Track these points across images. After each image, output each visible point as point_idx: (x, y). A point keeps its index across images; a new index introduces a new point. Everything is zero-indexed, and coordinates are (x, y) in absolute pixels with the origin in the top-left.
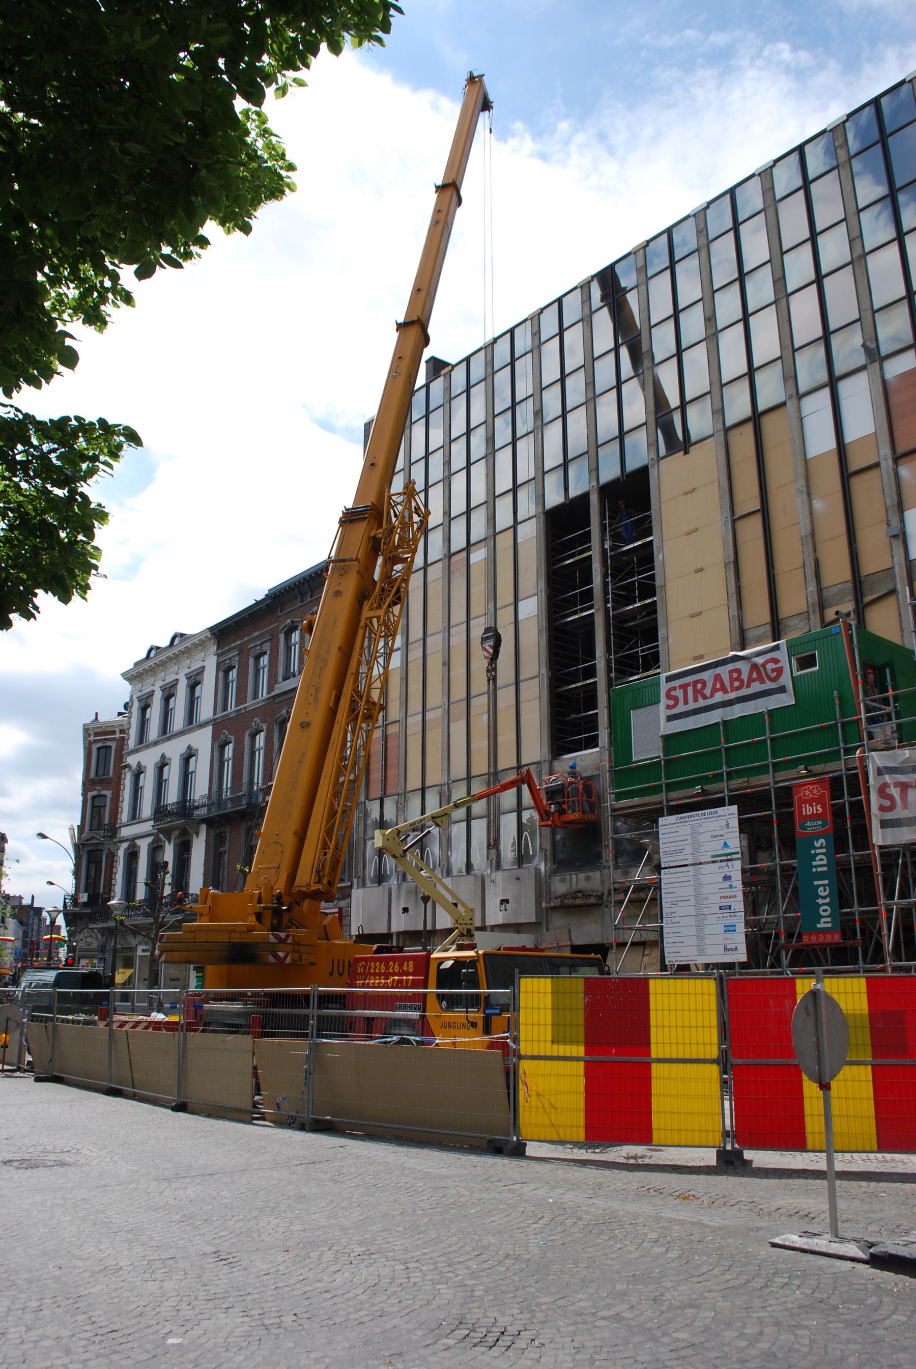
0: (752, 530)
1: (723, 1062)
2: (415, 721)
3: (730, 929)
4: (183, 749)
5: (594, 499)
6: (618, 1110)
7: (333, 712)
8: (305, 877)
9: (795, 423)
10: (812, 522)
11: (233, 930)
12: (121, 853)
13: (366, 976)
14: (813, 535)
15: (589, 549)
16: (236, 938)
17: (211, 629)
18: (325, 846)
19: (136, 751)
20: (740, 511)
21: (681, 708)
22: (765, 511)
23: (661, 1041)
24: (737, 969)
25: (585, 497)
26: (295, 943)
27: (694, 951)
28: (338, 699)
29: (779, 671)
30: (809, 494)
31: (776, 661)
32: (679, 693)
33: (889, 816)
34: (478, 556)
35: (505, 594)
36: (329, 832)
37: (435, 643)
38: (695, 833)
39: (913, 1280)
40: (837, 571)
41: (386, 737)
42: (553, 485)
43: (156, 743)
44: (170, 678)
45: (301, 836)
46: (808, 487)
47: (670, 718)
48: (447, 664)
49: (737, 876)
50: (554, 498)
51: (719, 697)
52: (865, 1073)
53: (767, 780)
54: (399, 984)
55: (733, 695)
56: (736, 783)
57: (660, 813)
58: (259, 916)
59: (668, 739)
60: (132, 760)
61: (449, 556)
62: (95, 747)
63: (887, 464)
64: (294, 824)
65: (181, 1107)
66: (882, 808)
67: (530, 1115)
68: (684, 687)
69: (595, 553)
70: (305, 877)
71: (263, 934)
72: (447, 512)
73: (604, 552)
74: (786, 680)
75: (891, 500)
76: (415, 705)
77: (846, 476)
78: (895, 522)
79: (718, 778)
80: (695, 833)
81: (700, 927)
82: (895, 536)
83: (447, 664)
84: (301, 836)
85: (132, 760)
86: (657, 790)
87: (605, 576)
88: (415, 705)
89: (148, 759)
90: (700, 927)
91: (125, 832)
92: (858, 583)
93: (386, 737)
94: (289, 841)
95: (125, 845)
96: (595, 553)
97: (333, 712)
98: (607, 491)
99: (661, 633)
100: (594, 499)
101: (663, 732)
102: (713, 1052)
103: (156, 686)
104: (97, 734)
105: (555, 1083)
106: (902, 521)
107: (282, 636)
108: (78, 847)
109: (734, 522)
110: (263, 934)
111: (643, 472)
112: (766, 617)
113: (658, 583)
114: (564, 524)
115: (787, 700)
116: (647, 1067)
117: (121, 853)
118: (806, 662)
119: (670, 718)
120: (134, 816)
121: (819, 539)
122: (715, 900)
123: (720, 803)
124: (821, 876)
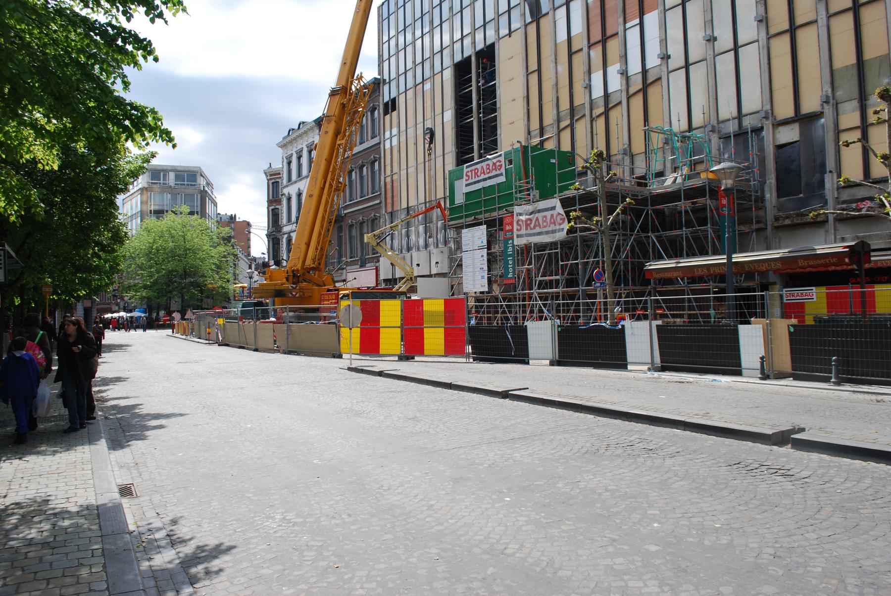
0: (534, 78)
1: (401, 327)
2: (404, 172)
3: (483, 277)
4: (297, 190)
5: (473, 59)
6: (370, 344)
7: (323, 189)
8: (309, 262)
9: (552, 24)
10: (557, 78)
11: (276, 285)
12: (284, 240)
13: (324, 300)
14: (557, 84)
15: (471, 86)
16: (277, 288)
17: (315, 121)
18: (317, 249)
19: (287, 186)
20: (530, 70)
21: (470, 181)
22: (539, 70)
23: (384, 320)
24: (682, 284)
25: (470, 57)
26: (300, 289)
27: (472, 287)
28: (325, 182)
29: (501, 166)
30: (556, 63)
31: (500, 161)
32: (470, 174)
33: (520, 233)
34: (428, 86)
35: (438, 110)
36: (318, 242)
37: (411, 131)
38: (473, 237)
39: (889, 467)
40: (565, 105)
41: (392, 181)
42: (479, 36)
43: (296, 182)
44: (299, 147)
45: (308, 245)
46: (556, 59)
47: (467, 185)
48: (416, 144)
49: (485, 255)
50: (458, 58)
51: (483, 176)
52: (359, 330)
53: (495, 214)
54: (331, 303)
55: (487, 176)
56: (487, 215)
57: (462, 227)
58: (287, 279)
59: (467, 194)
60: (286, 191)
61: (416, 86)
62: (271, 182)
63: (585, 49)
64: (305, 239)
65: (256, 350)
66: (517, 230)
67: (344, 346)
68: (471, 171)
69: (474, 88)
70: (309, 262)
71: (289, 286)
72: (414, 62)
73: (478, 87)
74: (503, 170)
75: (586, 68)
76: (404, 166)
77: (571, 54)
78: (587, 82)
79: (480, 213)
80: (473, 237)
81: (474, 276)
82: (760, 21)
83: (416, 144)
84: (308, 245)
85: (286, 191)
86: (461, 218)
87: (479, 100)
88: (404, 166)
89: (292, 190)
90: (474, 276)
91: (286, 229)
92: (572, 109)
93: (392, 181)
94: (303, 247)
95: (286, 236)
96: (474, 88)
97: (323, 189)
98: (480, 54)
99: (499, 131)
100: (473, 59)
101: (465, 192)
102: (399, 325)
103: (293, 150)
104: (271, 175)
105: (351, 337)
106: (590, 80)
107: (369, 114)
108: (268, 236)
109: (527, 75)
110: (289, 286)
111: (493, 45)
112: (538, 126)
113: (498, 106)
114: (462, 69)
115: (502, 179)
116: (422, 330)
117: (284, 240)
118: (510, 162)
119: (467, 185)
120: (289, 220)
121: (559, 86)
122: (479, 266)
123: (480, 224)
124: (510, 256)
